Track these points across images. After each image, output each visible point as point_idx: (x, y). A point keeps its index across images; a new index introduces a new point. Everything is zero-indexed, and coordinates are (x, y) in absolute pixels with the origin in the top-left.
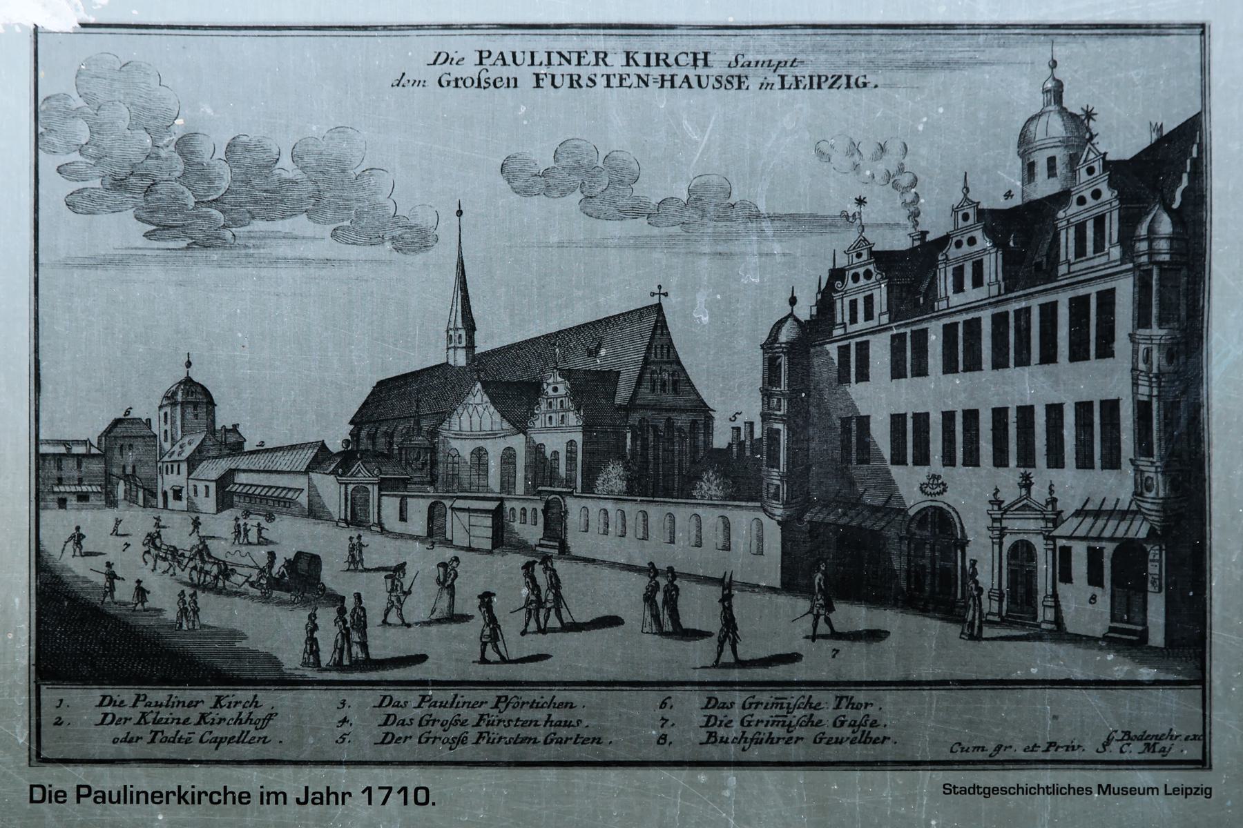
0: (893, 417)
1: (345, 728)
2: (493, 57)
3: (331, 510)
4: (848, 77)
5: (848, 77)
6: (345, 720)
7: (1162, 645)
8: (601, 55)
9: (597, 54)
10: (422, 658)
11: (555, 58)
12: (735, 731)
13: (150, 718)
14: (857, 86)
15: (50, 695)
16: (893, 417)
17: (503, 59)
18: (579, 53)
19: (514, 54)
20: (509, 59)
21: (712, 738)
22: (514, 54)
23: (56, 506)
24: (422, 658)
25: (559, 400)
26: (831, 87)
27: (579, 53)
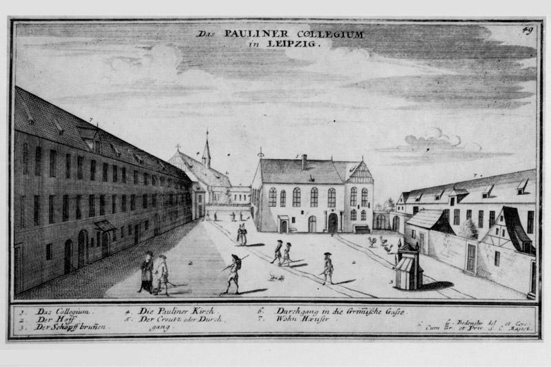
0: (491, 212)
1: (129, 315)
2: (231, 34)
3: (534, 245)
4: (305, 42)
5: (305, 42)
6: (128, 312)
7: (424, 284)
8: (284, 32)
9: (283, 32)
10: (447, 285)
11: (261, 34)
12: (51, 324)
13: (198, 311)
14: (310, 45)
15: (17, 310)
16: (491, 212)
17: (236, 34)
18: (274, 31)
19: (241, 32)
20: (239, 33)
21: (40, 327)
22: (241, 32)
23: (72, 240)
24: (447, 285)
25: (199, 194)
26: (296, 46)
27: (274, 31)
